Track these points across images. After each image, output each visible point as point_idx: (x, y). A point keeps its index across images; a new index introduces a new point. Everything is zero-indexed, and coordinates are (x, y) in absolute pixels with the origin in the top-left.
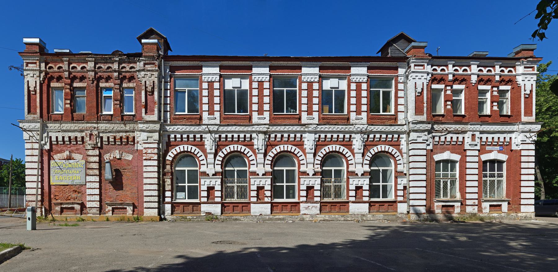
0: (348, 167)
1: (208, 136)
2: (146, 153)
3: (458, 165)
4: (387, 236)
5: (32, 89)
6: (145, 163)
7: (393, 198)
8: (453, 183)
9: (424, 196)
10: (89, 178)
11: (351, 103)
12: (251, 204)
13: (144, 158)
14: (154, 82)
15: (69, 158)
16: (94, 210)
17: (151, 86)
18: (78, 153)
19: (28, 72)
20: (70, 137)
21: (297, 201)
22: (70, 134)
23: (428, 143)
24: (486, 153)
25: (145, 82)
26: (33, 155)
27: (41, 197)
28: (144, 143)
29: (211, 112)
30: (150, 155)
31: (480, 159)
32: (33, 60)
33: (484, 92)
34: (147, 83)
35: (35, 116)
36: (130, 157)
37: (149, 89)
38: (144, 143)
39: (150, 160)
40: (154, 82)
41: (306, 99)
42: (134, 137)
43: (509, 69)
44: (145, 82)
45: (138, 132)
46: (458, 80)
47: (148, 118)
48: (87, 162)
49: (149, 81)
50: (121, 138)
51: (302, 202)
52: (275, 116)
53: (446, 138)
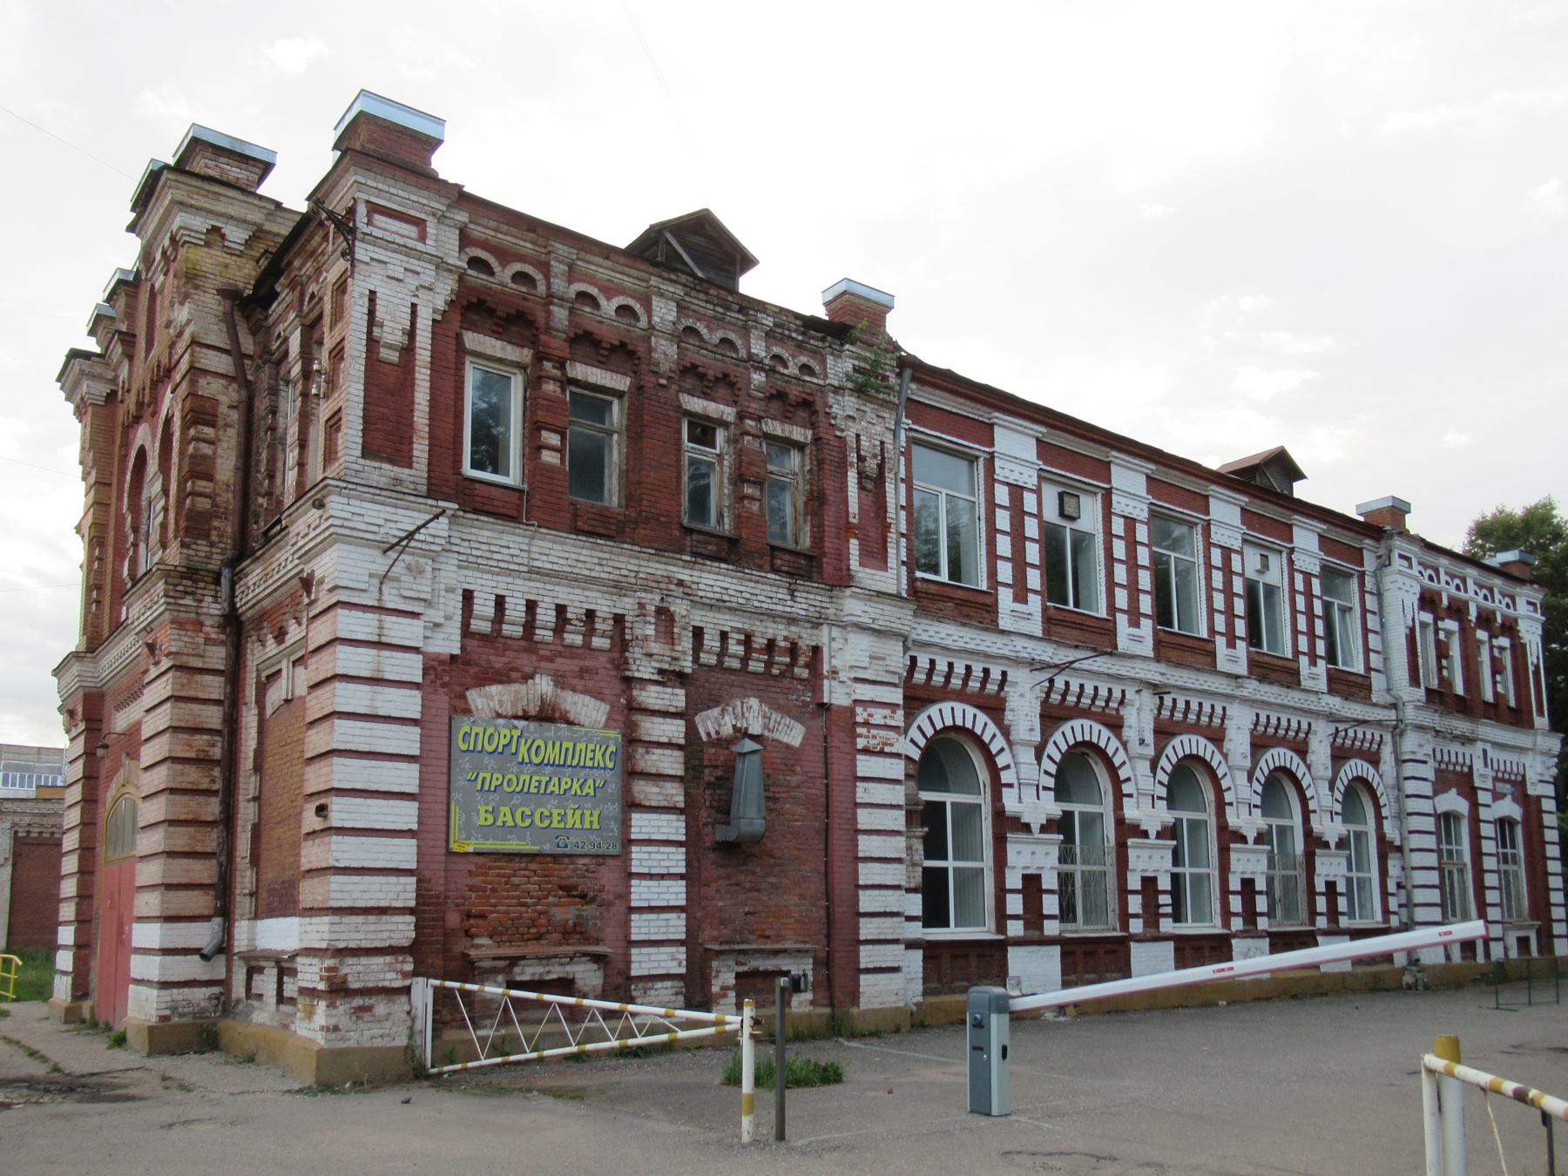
0: (1118, 806)
1: (1018, 676)
2: (866, 724)
3: (1519, 830)
4: (1273, 980)
5: (392, 334)
6: (866, 766)
7: (1379, 917)
8: (1461, 871)
9: (407, 740)
10: (642, 825)
11: (1009, 912)
12: (1458, 550)
13: (861, 743)
14: (882, 443)
15: (547, 715)
16: (665, 989)
17: (875, 456)
18: (585, 692)
19: (381, 254)
20: (561, 610)
21: (1219, 930)
22: (564, 594)
23: (435, 615)
24: (928, 942)
25: (858, 436)
26: (827, 806)
27: (1328, 902)
28: (857, 680)
29: (1541, 713)
30: (883, 733)
31: (691, 730)
32: (1506, 887)
33: (704, 430)
34: (865, 443)
35: (403, 473)
36: (794, 734)
37: (871, 465)
38: (857, 680)
39: (881, 753)
40: (882, 443)
41: (411, 919)
42: (816, 650)
43: (518, 267)
44: (858, 436)
45: (836, 632)
46: (935, 847)
47: (867, 577)
48: (632, 740)
49: (870, 438)
50: (771, 645)
51: (1235, 936)
52: (376, 529)
53: (1045, 788)
